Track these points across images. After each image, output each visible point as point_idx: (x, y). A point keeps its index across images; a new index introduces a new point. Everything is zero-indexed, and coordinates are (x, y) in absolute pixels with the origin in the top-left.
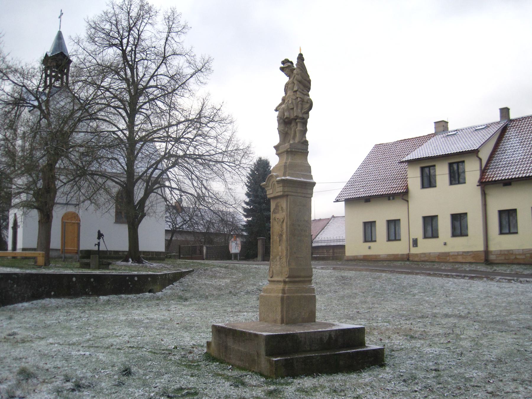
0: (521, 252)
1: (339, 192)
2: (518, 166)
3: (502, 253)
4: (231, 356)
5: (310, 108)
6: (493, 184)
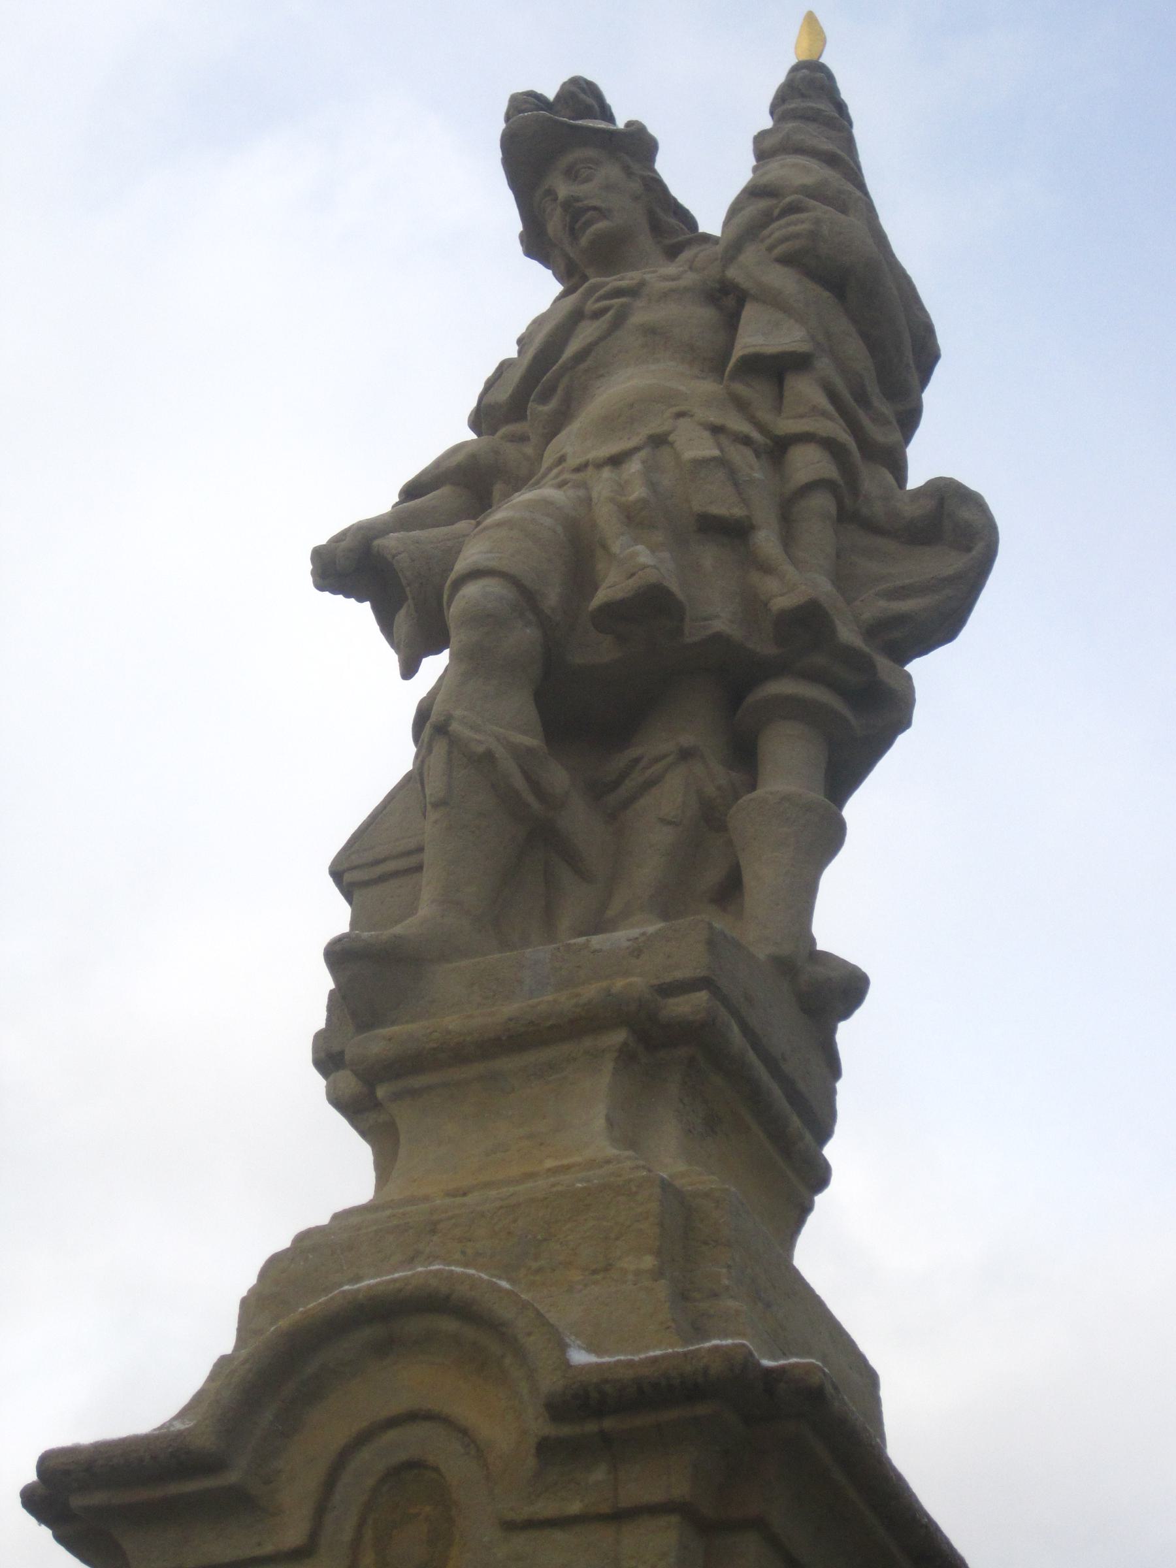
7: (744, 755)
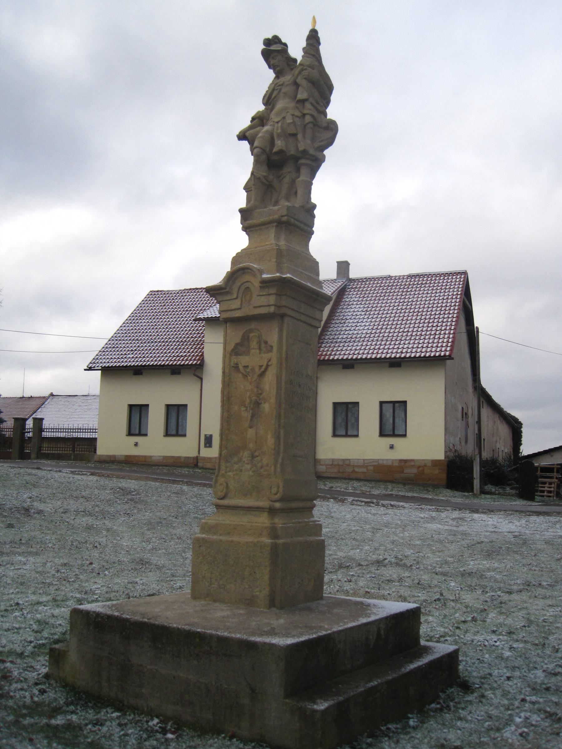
0: (361, 463)
1: (93, 355)
2: (365, 343)
3: (336, 463)
4: (144, 691)
5: (330, 142)
6: (329, 364)
7: (298, 170)
